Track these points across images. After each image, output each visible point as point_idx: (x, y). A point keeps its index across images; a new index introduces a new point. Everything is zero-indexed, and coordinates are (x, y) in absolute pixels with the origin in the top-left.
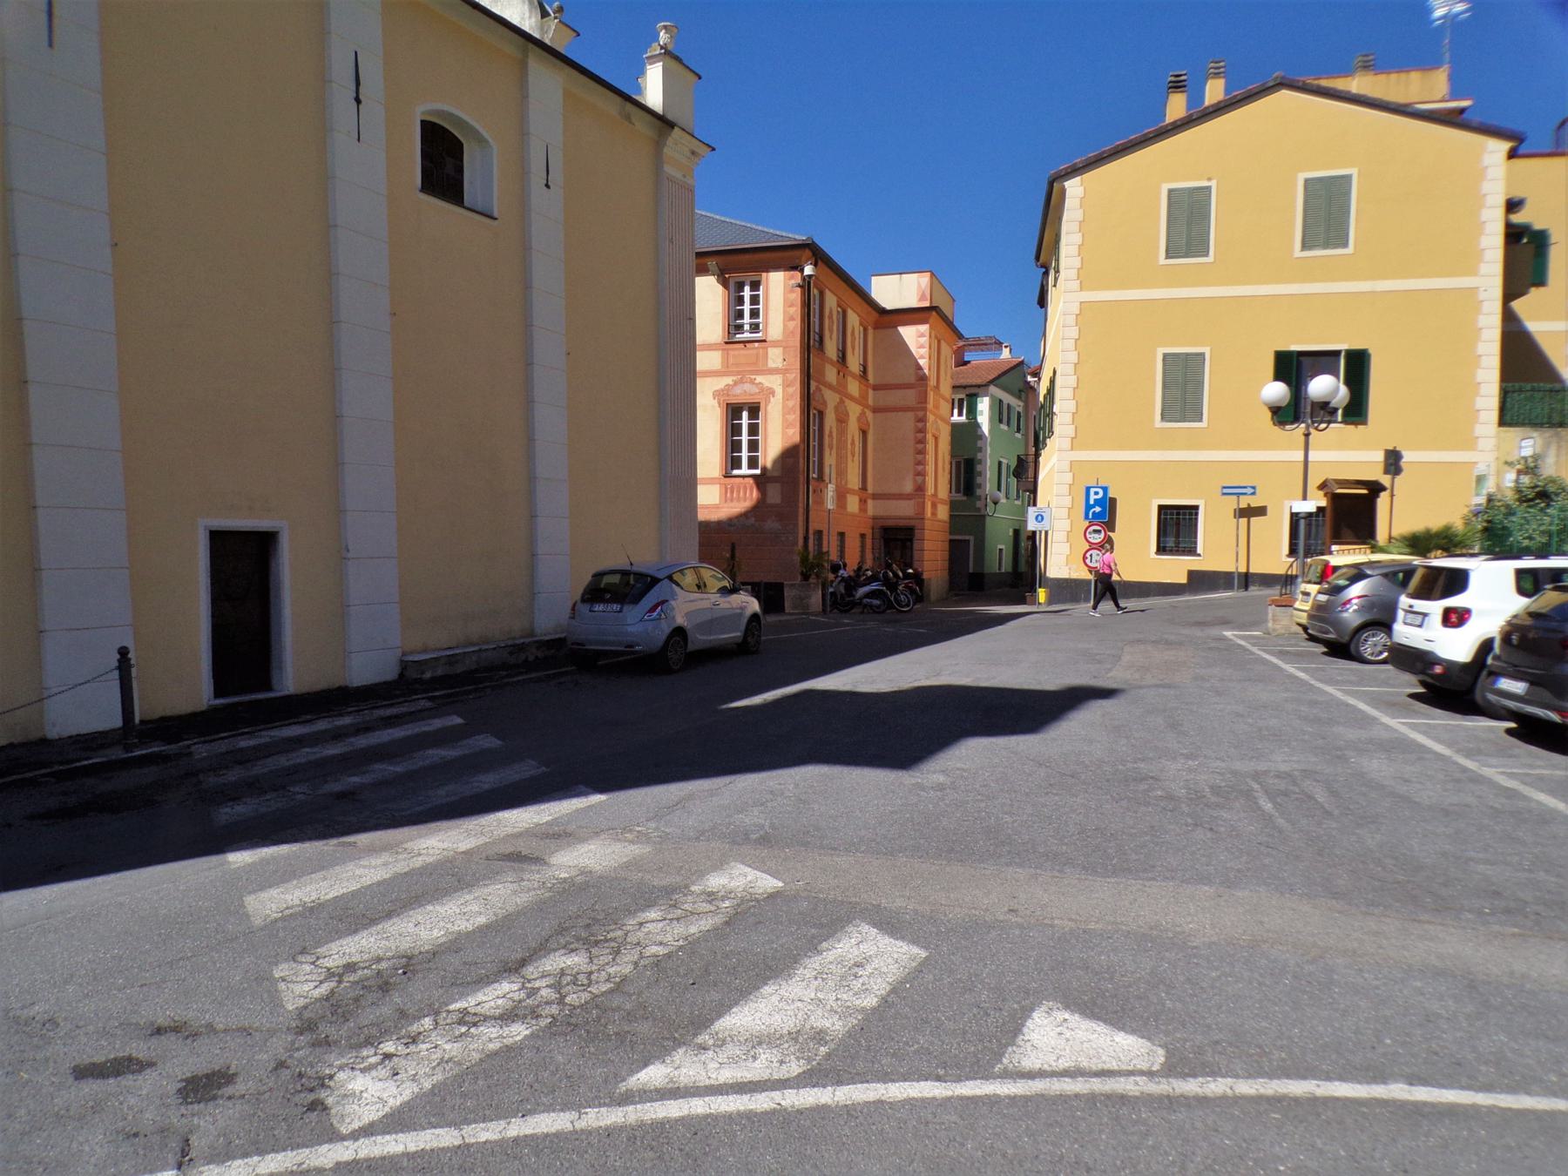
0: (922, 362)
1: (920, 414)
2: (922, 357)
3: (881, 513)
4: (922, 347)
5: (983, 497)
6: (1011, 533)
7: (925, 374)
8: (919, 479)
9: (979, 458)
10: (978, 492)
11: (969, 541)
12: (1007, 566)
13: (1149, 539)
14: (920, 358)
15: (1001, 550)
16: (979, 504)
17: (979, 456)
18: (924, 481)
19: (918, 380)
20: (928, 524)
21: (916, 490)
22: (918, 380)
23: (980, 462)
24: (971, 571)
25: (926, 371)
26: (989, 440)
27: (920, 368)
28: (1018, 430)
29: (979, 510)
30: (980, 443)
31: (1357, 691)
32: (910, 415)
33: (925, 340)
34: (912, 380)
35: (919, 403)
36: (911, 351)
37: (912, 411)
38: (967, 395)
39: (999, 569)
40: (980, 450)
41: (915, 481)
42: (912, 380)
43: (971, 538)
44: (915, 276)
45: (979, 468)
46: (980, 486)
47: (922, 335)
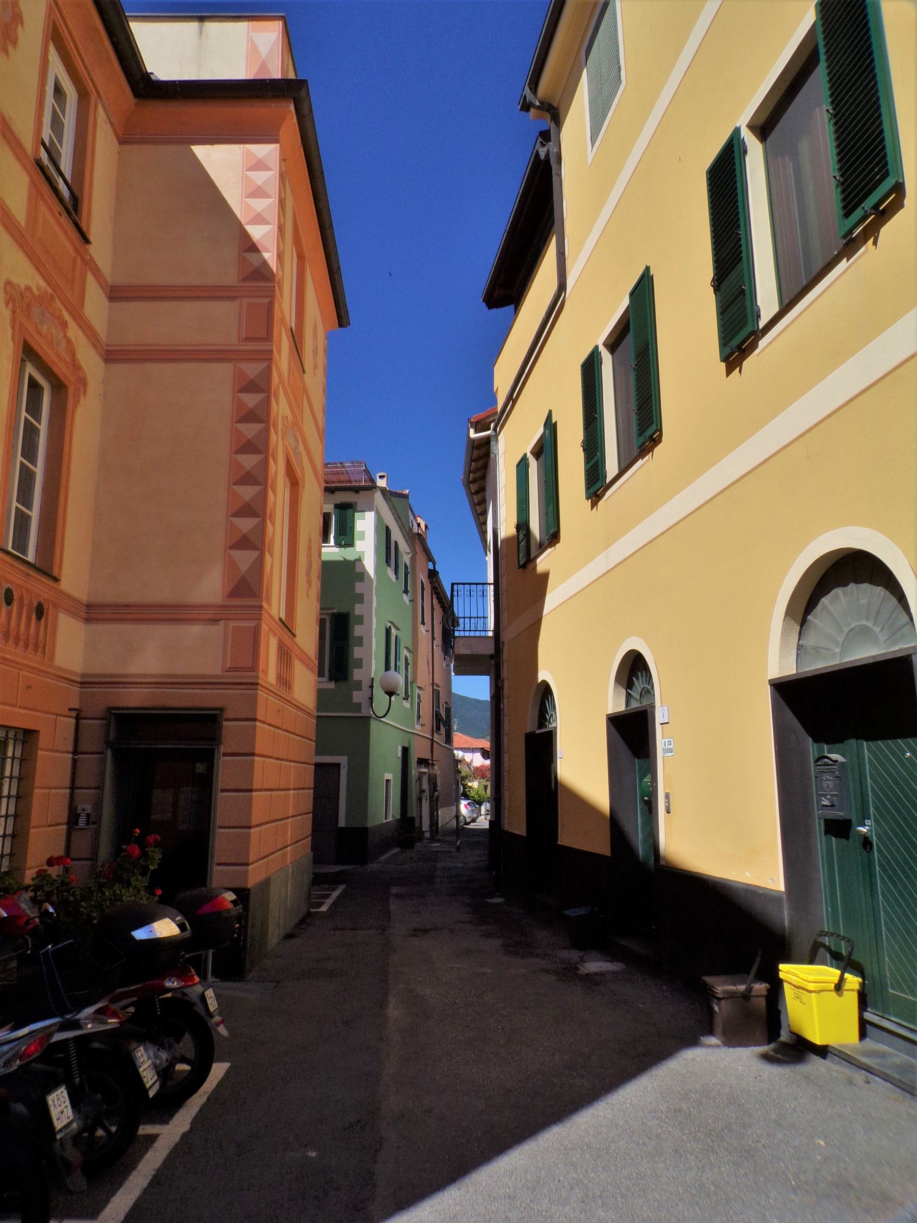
0: (257, 232)
1: (252, 370)
2: (259, 219)
3: (105, 665)
4: (258, 192)
5: (365, 686)
6: (400, 754)
7: (265, 263)
8: (244, 558)
9: (357, 612)
10: (357, 675)
11: (338, 765)
12: (394, 812)
13: (773, 776)
14: (248, 224)
15: (388, 781)
16: (358, 697)
17: (358, 609)
18: (259, 565)
19: (245, 279)
20: (266, 705)
21: (233, 594)
22: (245, 279)
23: (360, 620)
24: (342, 823)
25: (270, 256)
26: (375, 584)
27: (252, 247)
28: (406, 591)
29: (358, 707)
30: (359, 588)
31: (830, 976)
32: (223, 372)
33: (268, 178)
34: (231, 277)
35: (247, 339)
36: (235, 215)
37: (229, 360)
38: (337, 506)
39: (386, 818)
40: (360, 598)
41: (231, 564)
42: (231, 277)
43: (343, 760)
44: (242, 27)
45: (357, 630)
46: (359, 664)
47: (259, 166)
